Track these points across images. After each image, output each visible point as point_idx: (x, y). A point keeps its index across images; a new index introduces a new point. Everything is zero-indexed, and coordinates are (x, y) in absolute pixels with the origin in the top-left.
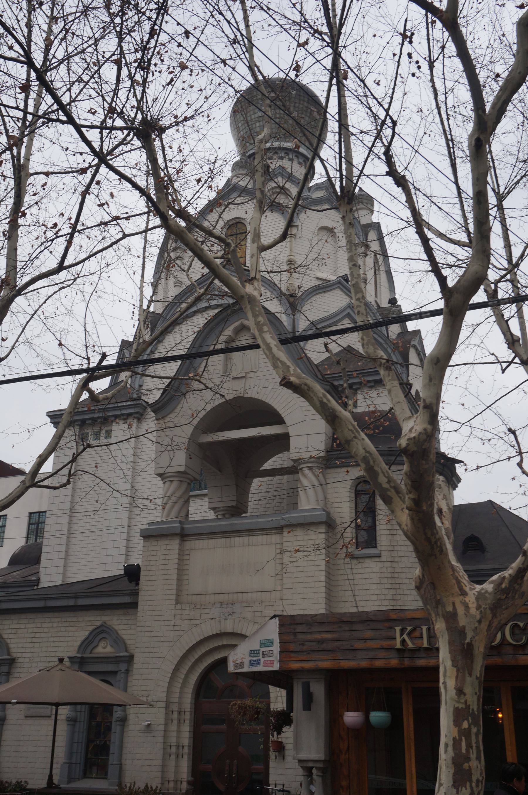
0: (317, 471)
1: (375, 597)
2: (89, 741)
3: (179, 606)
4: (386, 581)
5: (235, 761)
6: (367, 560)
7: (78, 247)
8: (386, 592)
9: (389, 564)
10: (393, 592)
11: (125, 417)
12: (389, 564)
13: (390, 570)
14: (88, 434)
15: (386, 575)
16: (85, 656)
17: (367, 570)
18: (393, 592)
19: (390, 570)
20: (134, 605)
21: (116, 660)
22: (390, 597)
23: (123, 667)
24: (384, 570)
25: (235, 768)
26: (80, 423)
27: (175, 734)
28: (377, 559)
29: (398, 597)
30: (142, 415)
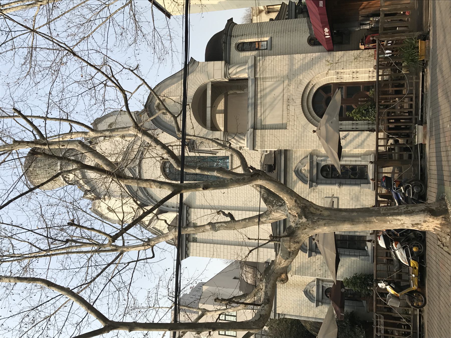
0: (230, 66)
1: (289, 39)
2: (350, 178)
3: (288, 128)
4: (282, 35)
5: (380, 285)
6: (272, 43)
7: (123, 35)
8: (287, 34)
9: (275, 34)
10: (287, 32)
11: (187, 241)
12: (275, 34)
13: (277, 33)
14: (193, 238)
15: (280, 35)
16: (309, 180)
17: (277, 43)
18: (287, 32)
19: (277, 33)
20: (286, 151)
21: (318, 286)
22: (289, 33)
23: (315, 157)
24: (277, 36)
25: (362, 99)
26: (187, 241)
27: (347, 126)
28: (273, 39)
29: (289, 30)
30: (188, 206)
